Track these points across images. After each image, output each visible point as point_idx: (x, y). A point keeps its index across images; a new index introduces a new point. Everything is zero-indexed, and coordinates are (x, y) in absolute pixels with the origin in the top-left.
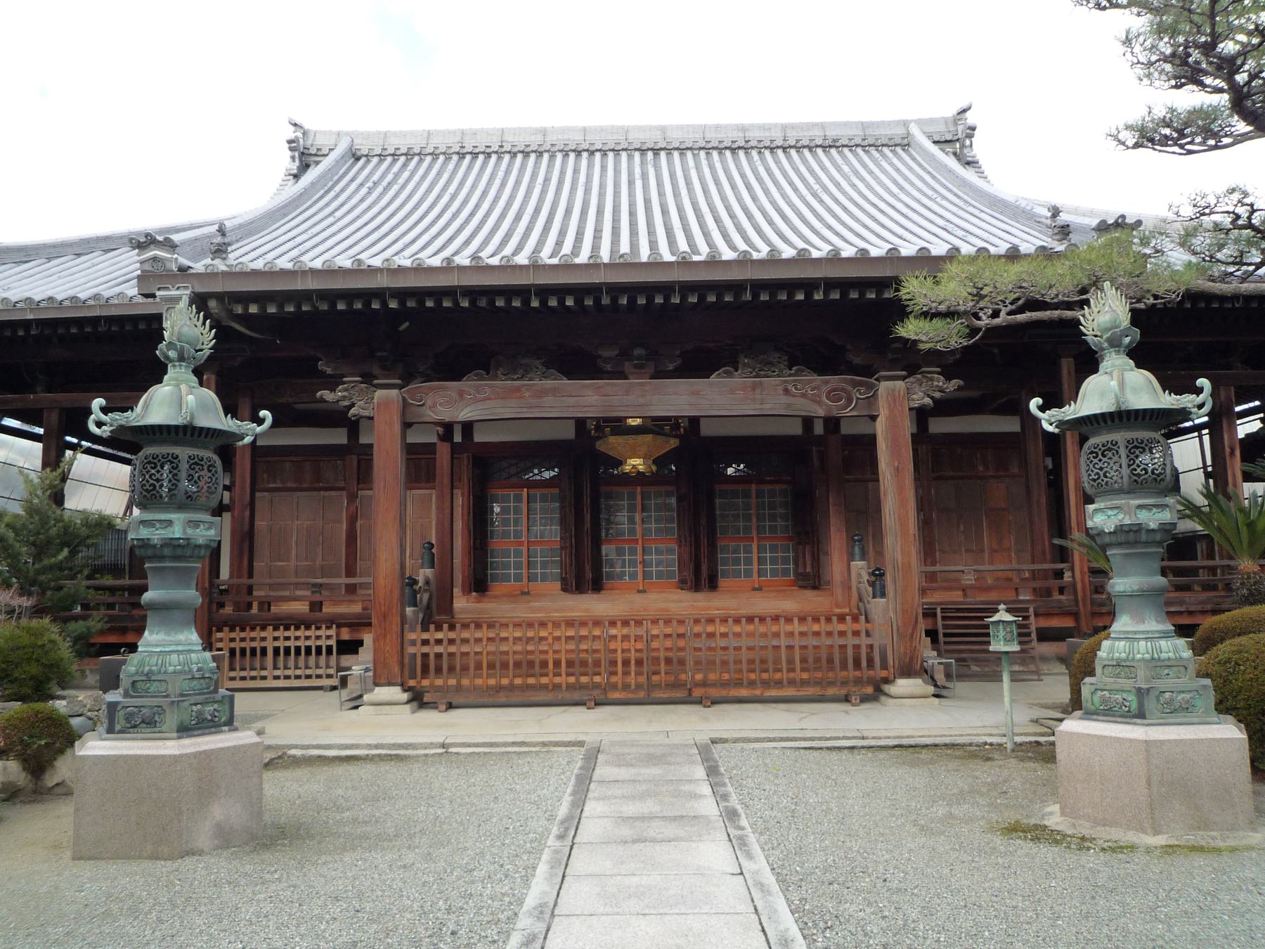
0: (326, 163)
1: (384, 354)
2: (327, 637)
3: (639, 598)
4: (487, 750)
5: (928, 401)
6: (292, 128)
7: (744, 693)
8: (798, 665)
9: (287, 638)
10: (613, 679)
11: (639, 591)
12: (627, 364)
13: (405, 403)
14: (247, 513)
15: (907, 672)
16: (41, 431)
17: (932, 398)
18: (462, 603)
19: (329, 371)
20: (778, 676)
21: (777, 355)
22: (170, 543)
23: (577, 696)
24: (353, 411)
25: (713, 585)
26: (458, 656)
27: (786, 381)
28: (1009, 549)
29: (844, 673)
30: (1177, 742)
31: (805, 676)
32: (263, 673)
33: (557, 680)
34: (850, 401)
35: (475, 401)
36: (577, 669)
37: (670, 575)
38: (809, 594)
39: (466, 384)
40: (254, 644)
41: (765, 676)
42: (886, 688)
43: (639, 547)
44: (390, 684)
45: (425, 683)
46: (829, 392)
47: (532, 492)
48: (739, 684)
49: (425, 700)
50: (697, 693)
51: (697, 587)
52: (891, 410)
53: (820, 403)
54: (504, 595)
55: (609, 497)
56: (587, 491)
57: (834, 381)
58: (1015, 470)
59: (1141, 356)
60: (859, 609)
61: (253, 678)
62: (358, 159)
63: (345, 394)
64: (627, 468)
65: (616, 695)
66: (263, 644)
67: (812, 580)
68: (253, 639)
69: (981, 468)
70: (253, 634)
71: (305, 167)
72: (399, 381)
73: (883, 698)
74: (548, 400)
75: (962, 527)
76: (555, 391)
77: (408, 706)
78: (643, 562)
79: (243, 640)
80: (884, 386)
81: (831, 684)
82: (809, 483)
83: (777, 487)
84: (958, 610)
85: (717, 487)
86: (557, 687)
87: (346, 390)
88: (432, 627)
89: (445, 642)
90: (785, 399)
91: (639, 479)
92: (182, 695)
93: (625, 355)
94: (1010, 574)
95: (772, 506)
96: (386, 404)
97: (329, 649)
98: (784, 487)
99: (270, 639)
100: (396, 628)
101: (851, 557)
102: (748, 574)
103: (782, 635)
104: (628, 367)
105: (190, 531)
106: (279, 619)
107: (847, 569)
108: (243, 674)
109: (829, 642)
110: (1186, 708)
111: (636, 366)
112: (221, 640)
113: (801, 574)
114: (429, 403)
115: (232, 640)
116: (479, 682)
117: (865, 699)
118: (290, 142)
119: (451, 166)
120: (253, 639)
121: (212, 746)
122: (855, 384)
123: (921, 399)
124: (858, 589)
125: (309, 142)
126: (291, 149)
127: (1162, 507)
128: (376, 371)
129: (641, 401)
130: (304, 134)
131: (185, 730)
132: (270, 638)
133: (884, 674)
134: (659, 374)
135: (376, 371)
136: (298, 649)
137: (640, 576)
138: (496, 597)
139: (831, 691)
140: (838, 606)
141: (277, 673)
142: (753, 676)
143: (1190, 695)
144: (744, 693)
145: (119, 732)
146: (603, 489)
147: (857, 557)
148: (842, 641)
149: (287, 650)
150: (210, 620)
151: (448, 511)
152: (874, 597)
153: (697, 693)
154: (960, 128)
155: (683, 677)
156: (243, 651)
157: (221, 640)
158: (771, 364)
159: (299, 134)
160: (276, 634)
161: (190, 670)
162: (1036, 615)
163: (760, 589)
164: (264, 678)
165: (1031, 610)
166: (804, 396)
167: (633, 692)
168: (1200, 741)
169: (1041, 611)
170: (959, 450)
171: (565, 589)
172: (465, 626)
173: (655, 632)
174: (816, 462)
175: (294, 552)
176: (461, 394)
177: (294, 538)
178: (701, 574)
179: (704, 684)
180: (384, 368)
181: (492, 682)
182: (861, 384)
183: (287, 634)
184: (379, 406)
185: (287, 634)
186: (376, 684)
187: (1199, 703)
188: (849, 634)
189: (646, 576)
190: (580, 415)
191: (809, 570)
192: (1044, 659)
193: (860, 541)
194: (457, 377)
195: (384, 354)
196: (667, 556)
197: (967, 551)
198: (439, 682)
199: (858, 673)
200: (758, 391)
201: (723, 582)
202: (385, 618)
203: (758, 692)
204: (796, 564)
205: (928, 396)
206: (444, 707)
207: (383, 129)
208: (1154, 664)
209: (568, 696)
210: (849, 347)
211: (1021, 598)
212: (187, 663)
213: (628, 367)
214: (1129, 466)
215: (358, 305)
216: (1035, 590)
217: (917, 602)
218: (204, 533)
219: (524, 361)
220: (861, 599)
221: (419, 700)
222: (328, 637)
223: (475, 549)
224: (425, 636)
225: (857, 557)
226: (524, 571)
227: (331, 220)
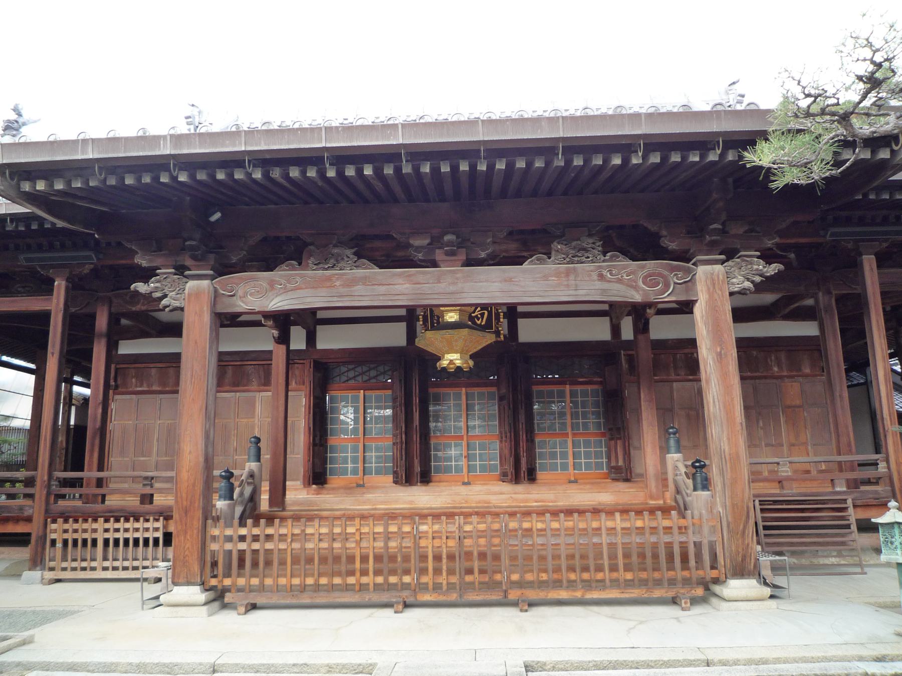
1: (194, 243)
2: (154, 529)
3: (463, 490)
5: (747, 284)
7: (563, 595)
8: (621, 561)
9: (117, 530)
10: (424, 579)
11: (464, 484)
12: (437, 251)
14: (100, 411)
15: (740, 572)
16: (33, 366)
17: (753, 282)
18: (297, 493)
19: (144, 263)
20: (600, 576)
21: (591, 241)
23: (385, 597)
24: (165, 302)
25: (531, 477)
26: (276, 552)
27: (600, 267)
28: (806, 444)
29: (671, 573)
31: (629, 576)
32: (94, 564)
33: (365, 580)
34: (667, 286)
35: (286, 291)
36: (385, 566)
37: (492, 468)
38: (622, 485)
39: (279, 274)
40: (85, 536)
41: (586, 576)
42: (717, 589)
43: (464, 443)
44: (189, 583)
45: (227, 582)
46: (645, 278)
47: (368, 393)
48: (557, 584)
49: (226, 600)
50: (513, 595)
51: (516, 479)
52: (711, 295)
53: (636, 288)
54: (339, 488)
55: (438, 399)
56: (416, 390)
57: (651, 265)
58: (807, 370)
60: (676, 501)
61: (84, 569)
63: (158, 285)
64: (444, 363)
65: (427, 597)
66: (94, 536)
67: (623, 473)
68: (85, 531)
69: (776, 369)
70: (85, 526)
72: (211, 272)
73: (714, 600)
74: (359, 289)
75: (761, 424)
76: (364, 280)
77: (205, 608)
78: (468, 457)
79: (76, 531)
80: (702, 271)
81: (658, 583)
82: (619, 378)
83: (589, 388)
84: (775, 502)
85: (536, 388)
86: (363, 588)
87: (158, 282)
88: (249, 522)
89: (249, 539)
90: (599, 285)
91: (456, 376)
93: (436, 242)
94: (807, 467)
95: (585, 416)
96: (197, 294)
97: (156, 541)
98: (595, 387)
99: (101, 530)
100: (197, 524)
101: (664, 450)
102: (565, 467)
103: (604, 531)
104: (439, 255)
106: (110, 511)
107: (661, 460)
108: (74, 564)
109: (653, 539)
111: (448, 254)
112: (55, 531)
113: (613, 468)
114: (240, 293)
115: (66, 531)
116: (283, 581)
117: (695, 601)
118: (187, 118)
120: (85, 531)
122: (672, 269)
123: (740, 282)
124: (675, 482)
128: (189, 262)
129: (452, 288)
130: (200, 112)
132: (99, 529)
133: (714, 574)
134: (470, 263)
135: (189, 262)
136: (126, 541)
137: (465, 470)
138: (333, 489)
139: (657, 593)
140: (652, 498)
141: (106, 564)
142: (572, 576)
144: (563, 595)
146: (432, 391)
147: (673, 449)
148: (667, 539)
149: (117, 541)
150: (47, 511)
151: (282, 408)
152: (695, 489)
153: (513, 595)
154: (731, 97)
155: (498, 577)
156: (75, 542)
157: (55, 531)
158: (585, 250)
160: (107, 526)
162: (855, 506)
163: (575, 481)
165: (850, 502)
166: (620, 281)
169: (859, 503)
170: (755, 353)
171: (396, 482)
172: (296, 518)
173: (468, 528)
174: (625, 365)
175: (155, 449)
176: (272, 284)
177: (156, 436)
178: (522, 469)
179: (520, 584)
180: (194, 258)
181: (296, 581)
182: (678, 269)
183: (117, 526)
184: (190, 295)
185: (117, 526)
186: (175, 584)
188: (675, 530)
189: (470, 469)
191: (621, 463)
192: (863, 550)
193: (674, 434)
194: (269, 266)
195: (194, 243)
196: (493, 450)
197: (767, 445)
198: (241, 582)
199: (686, 574)
200: (572, 277)
201: (540, 475)
202: (186, 513)
203: (578, 594)
204: (609, 458)
205: (748, 279)
206: (243, 609)
209: (376, 598)
210: (664, 233)
211: (838, 489)
213: (439, 255)
216: (848, 481)
217: (747, 492)
219: (336, 251)
220: (678, 492)
221: (219, 598)
222: (156, 529)
223: (314, 445)
224: (243, 531)
225: (673, 449)
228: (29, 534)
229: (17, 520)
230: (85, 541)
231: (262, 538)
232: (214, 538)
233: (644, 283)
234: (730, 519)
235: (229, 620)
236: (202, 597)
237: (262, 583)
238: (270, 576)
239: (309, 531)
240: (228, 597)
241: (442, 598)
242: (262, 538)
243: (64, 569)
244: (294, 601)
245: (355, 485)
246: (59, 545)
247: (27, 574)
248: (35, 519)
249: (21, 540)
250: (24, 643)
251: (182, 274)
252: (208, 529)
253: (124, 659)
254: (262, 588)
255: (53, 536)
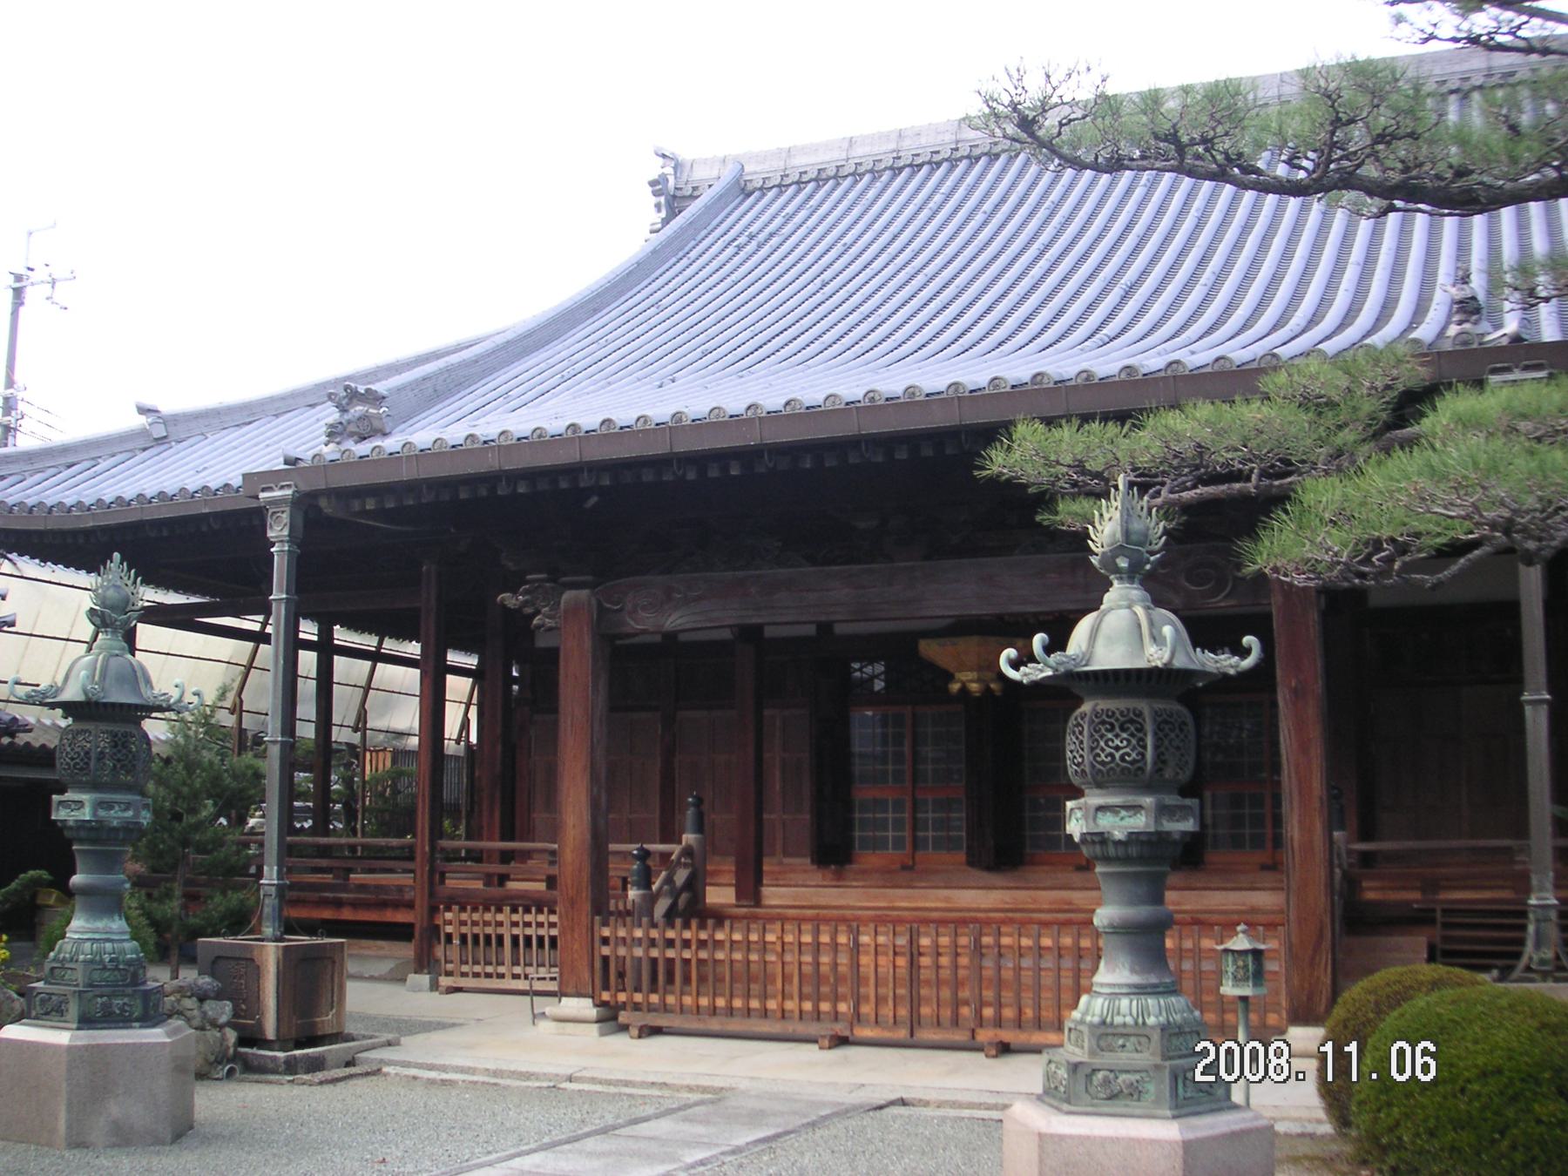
0: (693, 208)
4: (599, 1088)
6: (661, 160)
13: (601, 610)
22: (82, 825)
26: (694, 962)
30: (1083, 1140)
32: (501, 969)
45: (622, 997)
49: (621, 1019)
59: (1160, 586)
62: (749, 195)
71: (673, 213)
77: (596, 1026)
92: (91, 985)
99: (507, 924)
105: (102, 813)
110: (1135, 1092)
114: (629, 606)
118: (653, 184)
119: (879, 185)
121: (109, 1041)
125: (684, 178)
126: (656, 194)
127: (1135, 808)
130: (675, 168)
131: (86, 1022)
132: (506, 922)
136: (541, 939)
138: (864, 872)
143: (1137, 1077)
145: (36, 1018)
159: (669, 170)
161: (102, 961)
164: (502, 976)
167: (890, 1030)
168: (1115, 1140)
183: (528, 918)
187: (1151, 1087)
190: (823, 618)
207: (786, 145)
208: (1103, 1030)
212: (101, 952)
214: (1092, 749)
215: (483, 492)
218: (120, 814)
221: (610, 1019)
226: (907, 834)
227: (848, 239)
228: (411, 926)
229: (396, 905)
230: (488, 938)
231: (678, 943)
232: (605, 941)
233: (1188, 580)
234: (1294, 940)
235: (621, 1041)
236: (593, 1012)
237: (663, 1000)
238: (672, 993)
239: (720, 936)
240: (623, 1017)
241: (886, 1035)
242: (678, 943)
243: (464, 975)
244: (700, 1026)
245: (898, 866)
246: (456, 941)
247: (413, 978)
248: (418, 903)
249: (400, 933)
250: (389, 1044)
251: (555, 581)
252: (596, 927)
253: (481, 1066)
254: (665, 1008)
255: (449, 929)
